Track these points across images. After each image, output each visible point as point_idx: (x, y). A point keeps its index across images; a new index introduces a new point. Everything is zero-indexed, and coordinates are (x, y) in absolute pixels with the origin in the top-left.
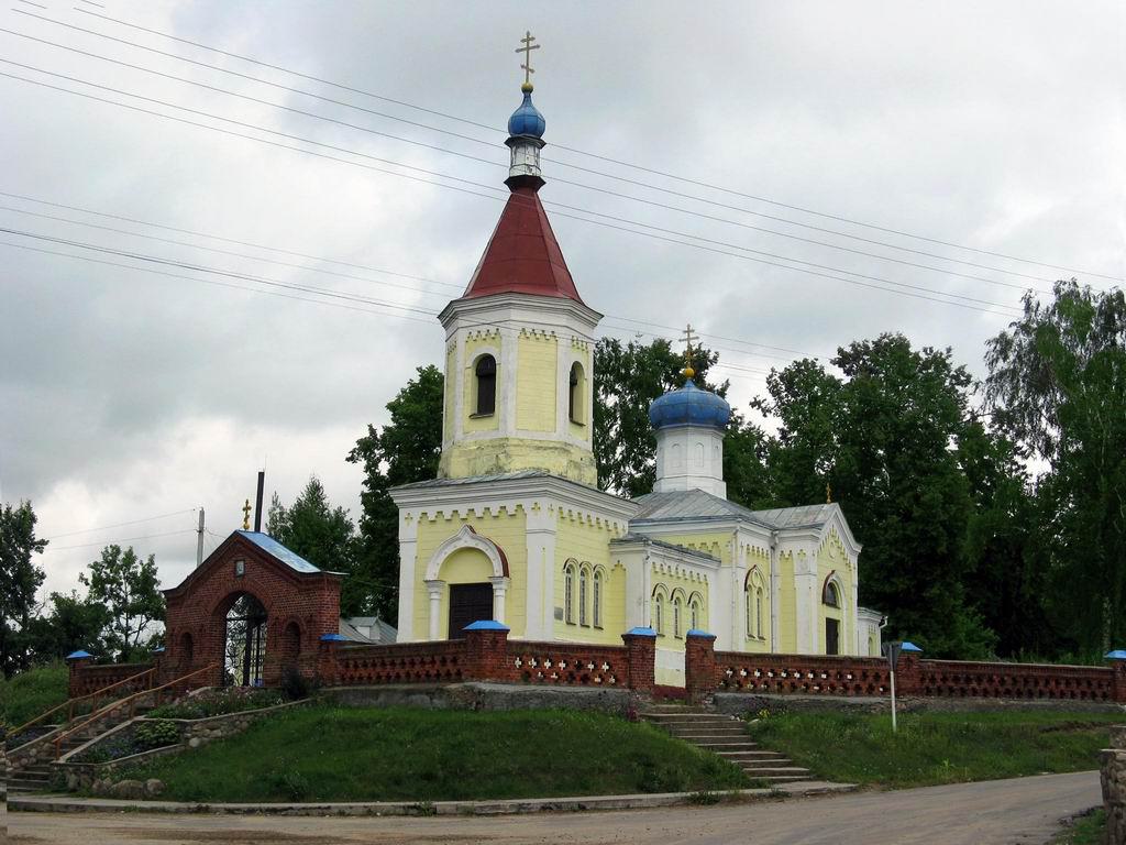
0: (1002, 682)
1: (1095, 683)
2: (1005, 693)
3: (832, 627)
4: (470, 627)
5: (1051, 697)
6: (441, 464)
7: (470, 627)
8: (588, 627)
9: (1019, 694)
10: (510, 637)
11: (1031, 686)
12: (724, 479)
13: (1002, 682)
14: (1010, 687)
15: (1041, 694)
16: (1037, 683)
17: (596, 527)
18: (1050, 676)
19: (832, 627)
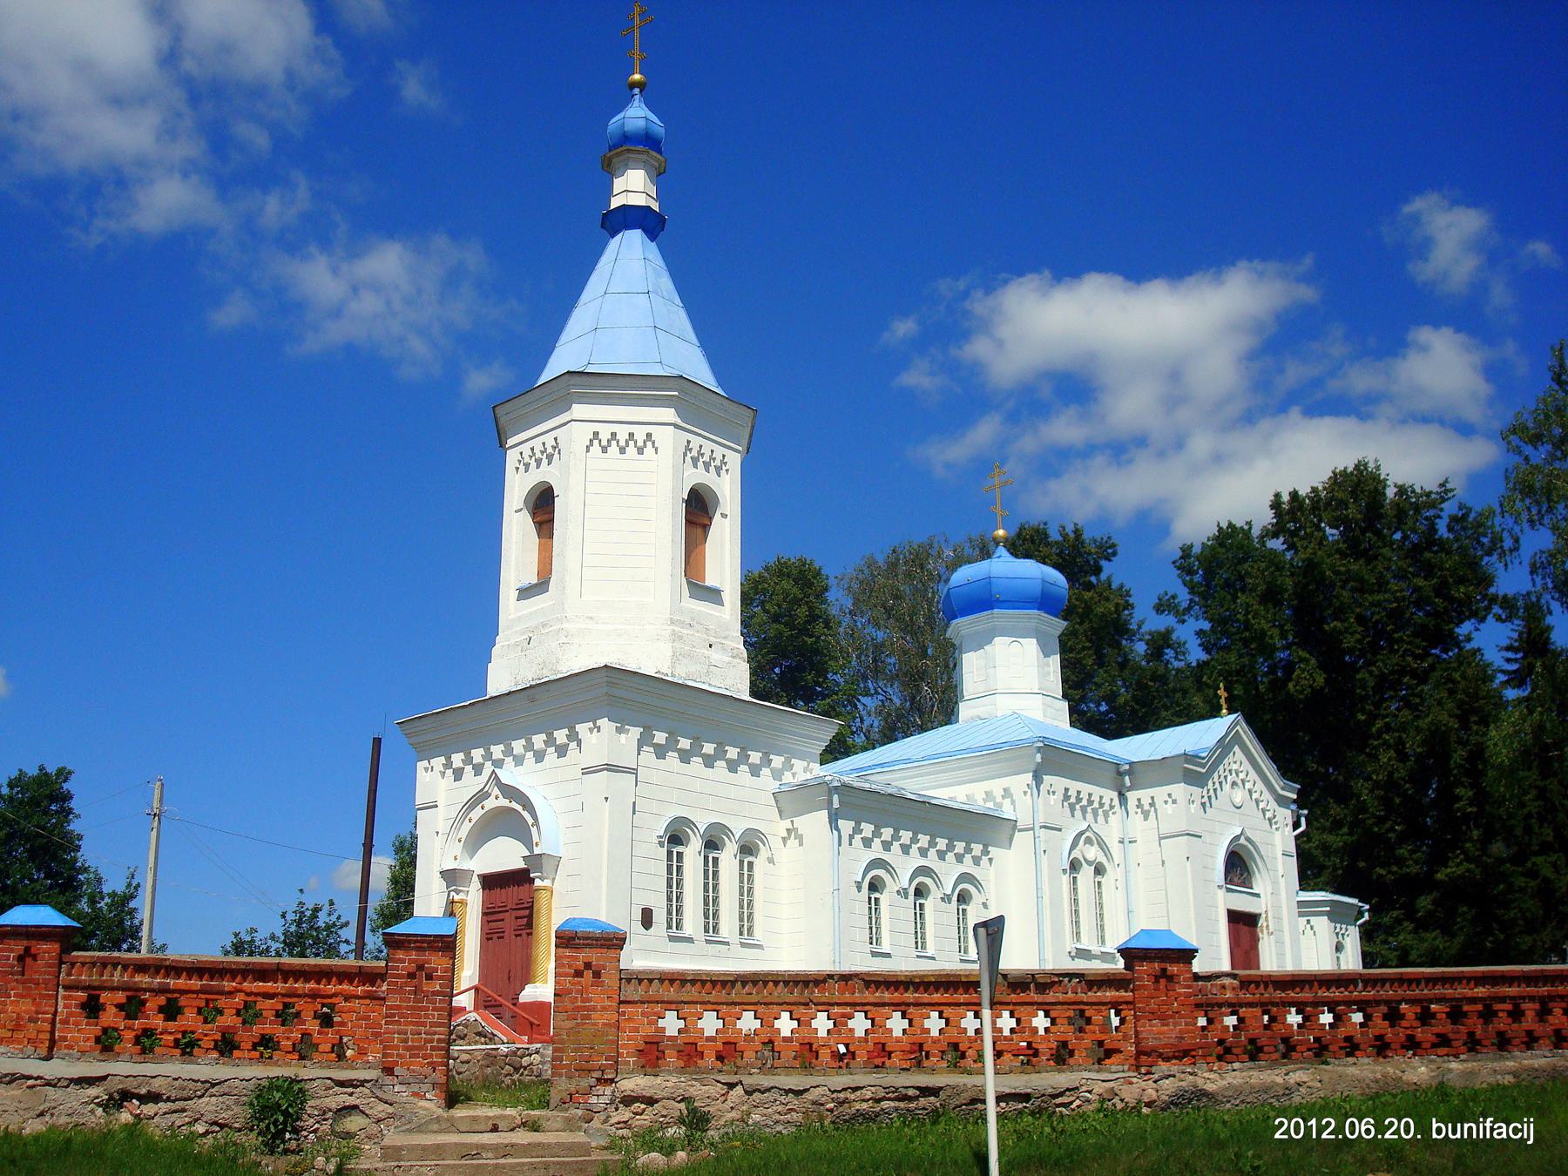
0: (1425, 1017)
1: (1530, 1008)
2: (1405, 1047)
3: (1243, 925)
4: (79, 925)
5: (1557, 1046)
6: (1232, 268)
7: (79, 925)
8: (690, 940)
9: (1473, 1045)
10: (1198, 966)
11: (1502, 1023)
12: (1065, 696)
13: (1425, 1017)
14: (1448, 1028)
15: (1530, 1041)
16: (1516, 1015)
17: (509, 760)
18: (1551, 998)
19: (1243, 925)
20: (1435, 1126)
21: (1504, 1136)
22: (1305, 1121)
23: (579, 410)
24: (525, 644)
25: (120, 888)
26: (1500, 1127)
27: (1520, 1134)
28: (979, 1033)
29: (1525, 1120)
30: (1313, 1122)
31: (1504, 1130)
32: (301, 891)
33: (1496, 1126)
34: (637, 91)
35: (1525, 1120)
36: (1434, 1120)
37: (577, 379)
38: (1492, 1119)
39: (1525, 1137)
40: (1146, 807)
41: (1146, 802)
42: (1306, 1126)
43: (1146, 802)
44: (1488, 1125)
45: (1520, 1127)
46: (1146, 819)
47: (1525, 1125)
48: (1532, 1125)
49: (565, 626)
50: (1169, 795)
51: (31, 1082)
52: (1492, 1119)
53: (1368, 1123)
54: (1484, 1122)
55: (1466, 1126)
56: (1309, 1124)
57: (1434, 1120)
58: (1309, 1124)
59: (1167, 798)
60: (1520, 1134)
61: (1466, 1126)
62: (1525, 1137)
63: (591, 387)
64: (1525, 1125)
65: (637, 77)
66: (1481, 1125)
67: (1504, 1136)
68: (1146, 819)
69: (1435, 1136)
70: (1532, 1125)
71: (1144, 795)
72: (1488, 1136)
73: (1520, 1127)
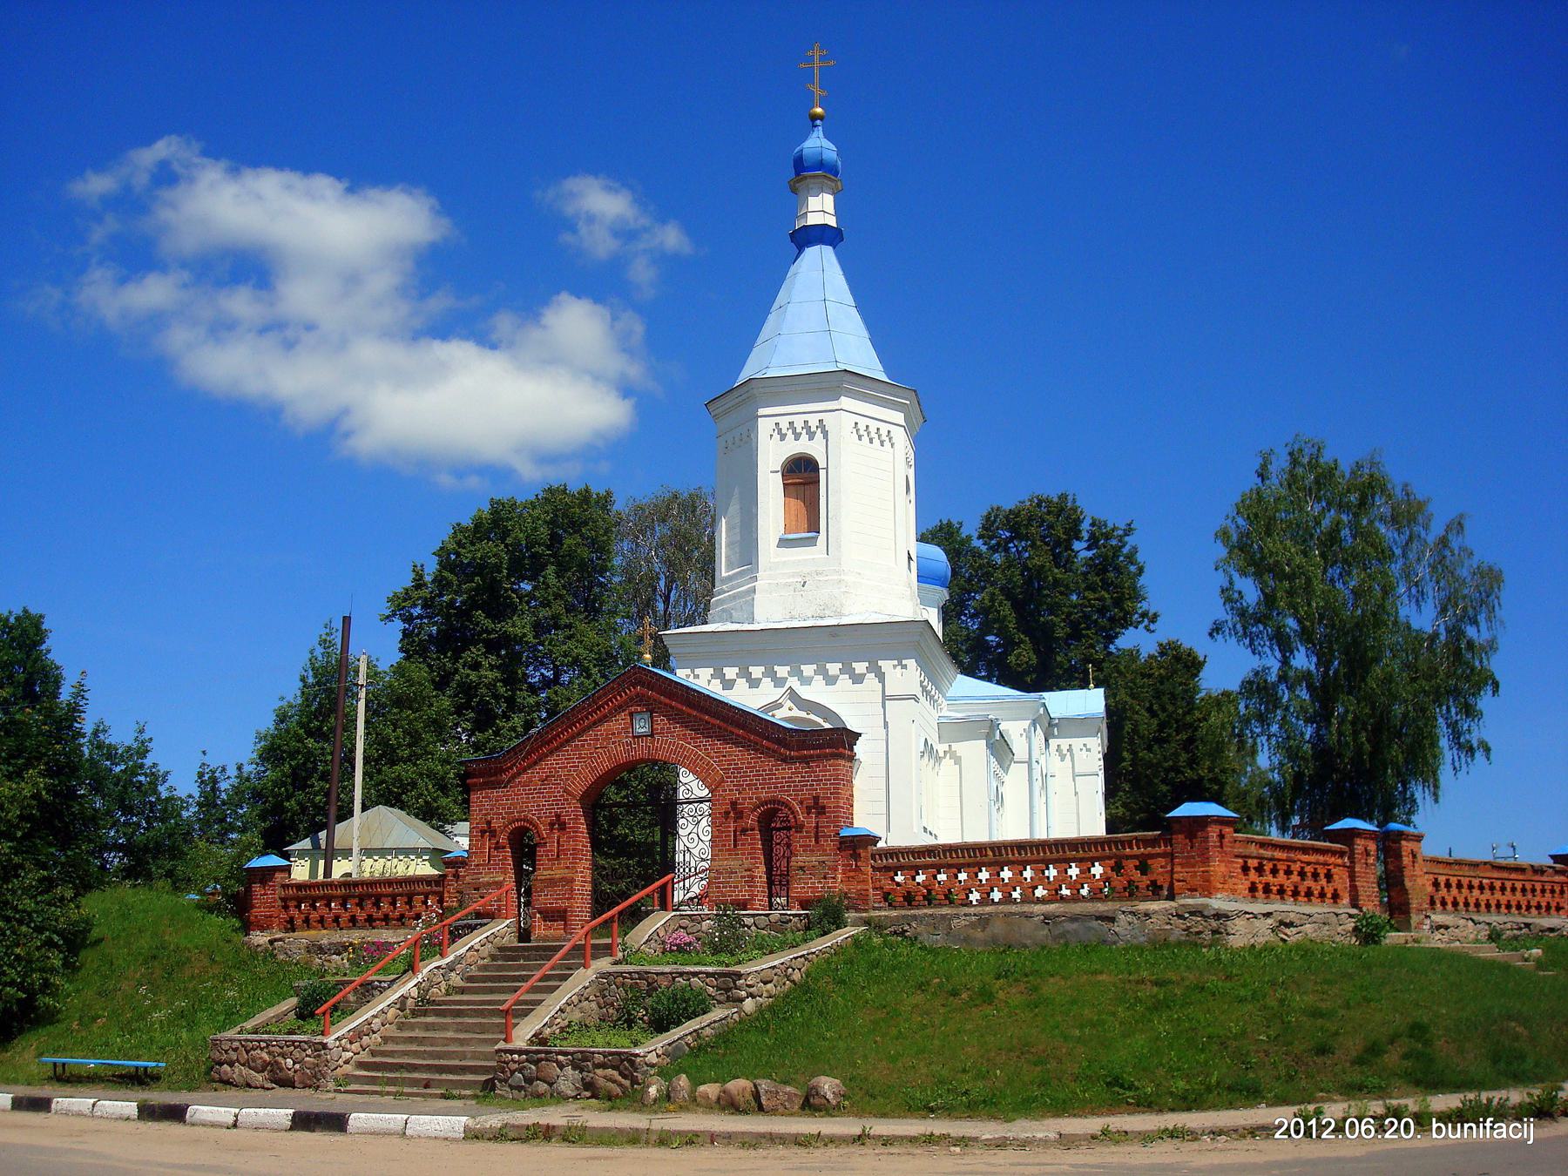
20: (1435, 1126)
21: (1504, 1136)
22: (1306, 1122)
23: (846, 402)
24: (799, 586)
25: (129, 740)
26: (1501, 1127)
27: (1520, 1134)
28: (21, 1102)
29: (1525, 1119)
30: (1313, 1122)
31: (1504, 1130)
32: (204, 753)
33: (1495, 1126)
34: (818, 122)
35: (1525, 1119)
36: (1434, 1120)
37: (848, 377)
38: (1492, 1119)
39: (1525, 1136)
40: (1065, 752)
41: (1065, 748)
42: (1305, 1125)
43: (1065, 748)
44: (1488, 1124)
45: (1520, 1126)
46: (1062, 760)
47: (1525, 1125)
48: (1532, 1125)
49: (843, 577)
50: (1085, 745)
51: (1247, 916)
52: (1492, 1119)
53: (1368, 1123)
54: (1485, 1122)
55: (1466, 1126)
56: (1309, 1124)
57: (1434, 1120)
58: (1309, 1124)
59: (1082, 747)
60: (1520, 1134)
61: (1466, 1126)
62: (1525, 1136)
63: (859, 386)
64: (1525, 1125)
65: (819, 110)
66: (1481, 1125)
67: (1504, 1136)
68: (1062, 760)
69: (1435, 1135)
70: (1532, 1125)
71: (1064, 743)
72: (1488, 1136)
73: (1520, 1126)
